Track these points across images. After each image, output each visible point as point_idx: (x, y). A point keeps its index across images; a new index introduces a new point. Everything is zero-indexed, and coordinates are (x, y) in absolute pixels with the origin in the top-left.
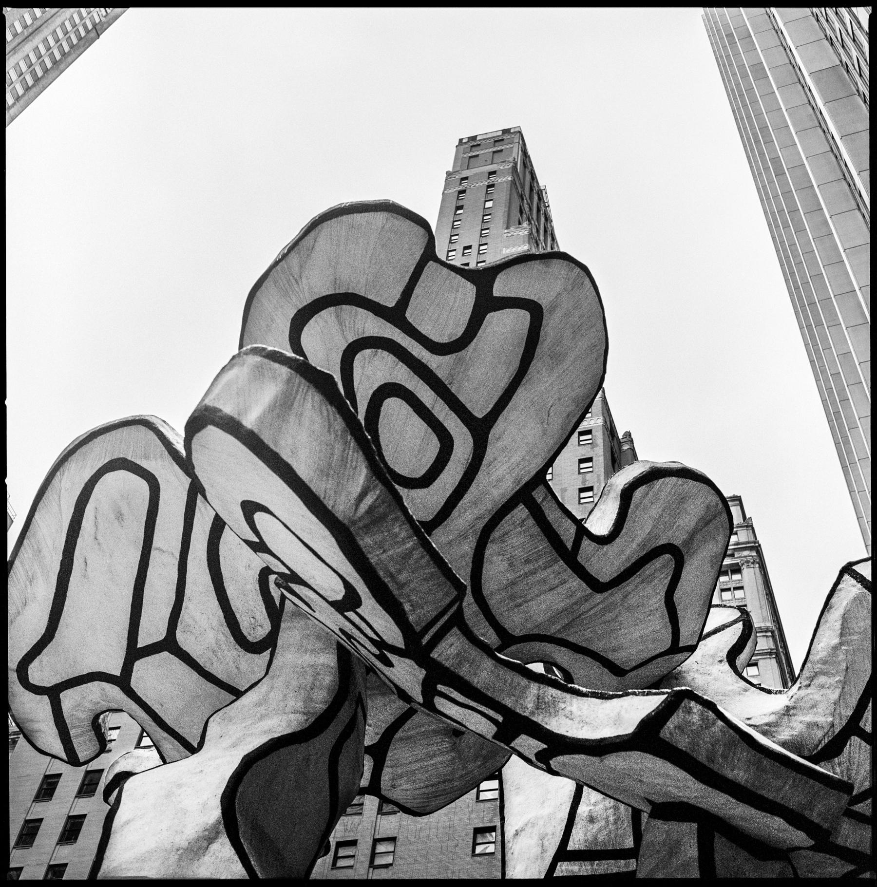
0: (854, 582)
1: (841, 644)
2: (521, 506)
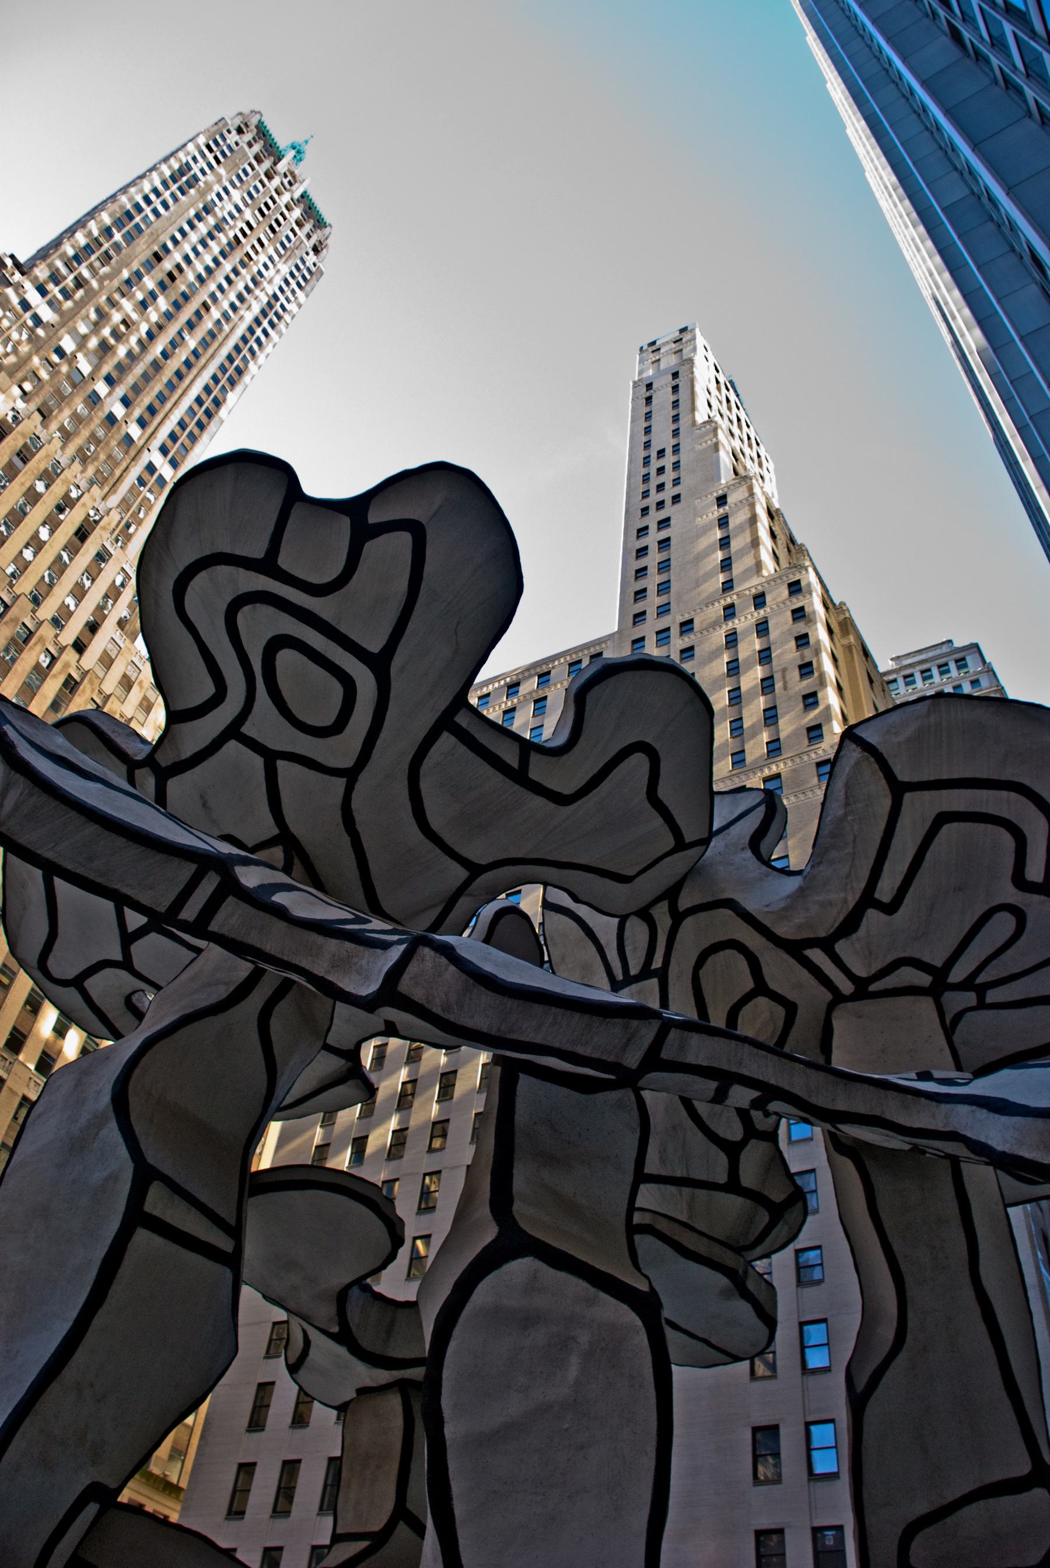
0: (854, 746)
1: (846, 815)
2: (445, 735)
